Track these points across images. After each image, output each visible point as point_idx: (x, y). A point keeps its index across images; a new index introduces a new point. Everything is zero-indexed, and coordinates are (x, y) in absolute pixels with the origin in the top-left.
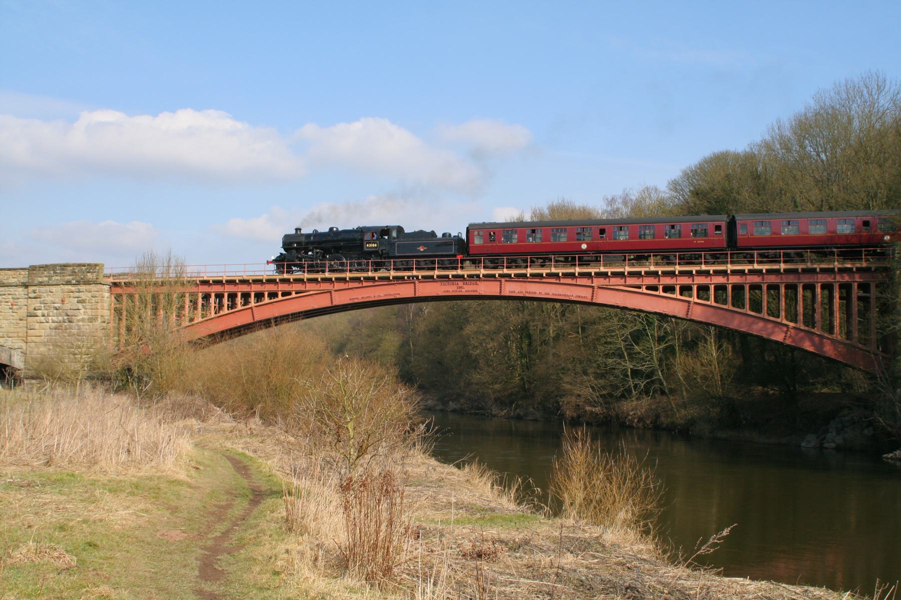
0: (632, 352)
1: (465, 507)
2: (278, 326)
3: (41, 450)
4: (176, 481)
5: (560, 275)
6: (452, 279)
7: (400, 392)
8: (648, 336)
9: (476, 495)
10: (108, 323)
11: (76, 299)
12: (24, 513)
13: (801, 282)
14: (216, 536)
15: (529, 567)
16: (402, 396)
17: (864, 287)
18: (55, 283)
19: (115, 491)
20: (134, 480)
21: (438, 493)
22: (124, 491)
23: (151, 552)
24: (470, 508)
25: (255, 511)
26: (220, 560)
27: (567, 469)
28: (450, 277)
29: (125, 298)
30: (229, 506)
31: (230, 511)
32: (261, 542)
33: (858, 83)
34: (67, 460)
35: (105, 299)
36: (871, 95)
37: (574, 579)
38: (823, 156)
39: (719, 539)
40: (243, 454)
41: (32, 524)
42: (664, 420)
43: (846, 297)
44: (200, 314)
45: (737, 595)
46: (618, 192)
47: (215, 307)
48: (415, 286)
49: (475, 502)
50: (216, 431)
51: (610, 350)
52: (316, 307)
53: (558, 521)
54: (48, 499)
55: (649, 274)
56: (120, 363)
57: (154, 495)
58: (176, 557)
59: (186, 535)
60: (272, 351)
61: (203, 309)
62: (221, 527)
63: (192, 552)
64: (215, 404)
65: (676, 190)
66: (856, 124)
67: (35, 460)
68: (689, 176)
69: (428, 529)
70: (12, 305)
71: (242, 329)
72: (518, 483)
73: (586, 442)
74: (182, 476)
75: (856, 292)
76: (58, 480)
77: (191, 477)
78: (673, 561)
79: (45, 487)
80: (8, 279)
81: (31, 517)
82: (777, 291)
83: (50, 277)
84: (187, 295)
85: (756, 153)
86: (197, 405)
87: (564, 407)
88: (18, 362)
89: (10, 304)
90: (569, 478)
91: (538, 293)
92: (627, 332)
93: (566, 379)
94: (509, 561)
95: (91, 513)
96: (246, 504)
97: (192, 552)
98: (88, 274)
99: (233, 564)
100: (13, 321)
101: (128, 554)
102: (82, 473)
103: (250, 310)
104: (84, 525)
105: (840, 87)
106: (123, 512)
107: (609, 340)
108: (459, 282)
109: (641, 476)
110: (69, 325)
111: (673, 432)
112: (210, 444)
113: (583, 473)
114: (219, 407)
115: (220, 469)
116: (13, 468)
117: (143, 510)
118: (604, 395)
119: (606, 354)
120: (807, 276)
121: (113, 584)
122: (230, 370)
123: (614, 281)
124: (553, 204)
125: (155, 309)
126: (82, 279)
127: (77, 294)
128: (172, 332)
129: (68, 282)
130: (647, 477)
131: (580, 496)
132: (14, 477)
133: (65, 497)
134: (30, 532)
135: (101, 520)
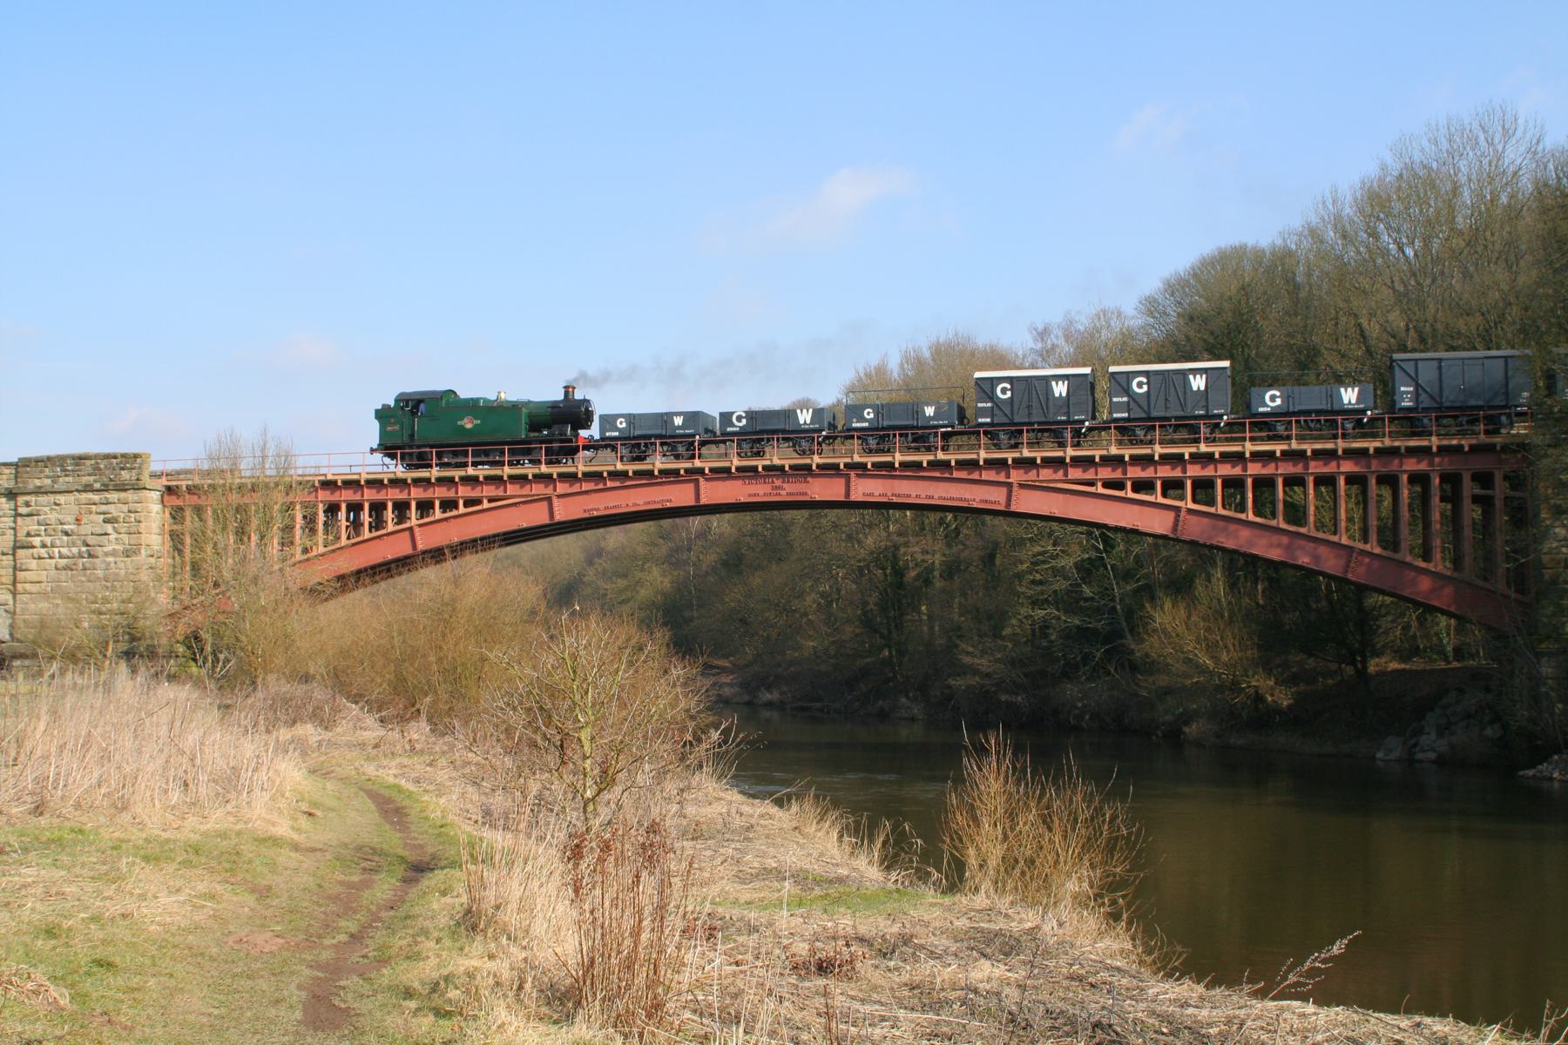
2: (458, 559)
4: (270, 838)
7: (674, 672)
9: (811, 854)
11: (102, 517)
14: (340, 942)
15: (914, 988)
16: (678, 679)
17: (1484, 479)
18: (64, 488)
19: (157, 859)
20: (194, 837)
21: (743, 852)
22: (173, 860)
24: (800, 877)
26: (344, 988)
27: (972, 805)
28: (760, 469)
29: (188, 513)
30: (366, 885)
33: (1471, 124)
35: (153, 515)
36: (1490, 143)
38: (1409, 252)
39: (1324, 961)
43: (1453, 499)
45: (1295, 1035)
46: (1055, 318)
49: (807, 867)
50: (351, 746)
53: (962, 900)
55: (1108, 461)
57: (228, 866)
59: (281, 941)
61: (326, 532)
63: (292, 973)
65: (1151, 314)
66: (1466, 197)
67: (16, 803)
68: (1175, 287)
69: (728, 917)
71: (393, 565)
74: (283, 829)
75: (1469, 488)
77: (298, 830)
78: (1170, 973)
79: (27, 853)
82: (1331, 488)
83: (55, 479)
85: (1293, 247)
90: (976, 821)
91: (914, 495)
94: (876, 977)
95: (108, 903)
97: (292, 973)
98: (123, 472)
99: (368, 997)
101: (172, 980)
102: (99, 827)
103: (407, 534)
104: (92, 927)
106: (168, 900)
107: (1038, 577)
109: (1104, 815)
112: (338, 769)
113: (1000, 811)
114: (356, 703)
117: (205, 894)
123: (1046, 473)
124: (938, 342)
125: (241, 533)
126: (111, 480)
127: (103, 508)
129: (86, 486)
130: (1113, 819)
131: (995, 853)
133: (63, 873)
135: (124, 916)
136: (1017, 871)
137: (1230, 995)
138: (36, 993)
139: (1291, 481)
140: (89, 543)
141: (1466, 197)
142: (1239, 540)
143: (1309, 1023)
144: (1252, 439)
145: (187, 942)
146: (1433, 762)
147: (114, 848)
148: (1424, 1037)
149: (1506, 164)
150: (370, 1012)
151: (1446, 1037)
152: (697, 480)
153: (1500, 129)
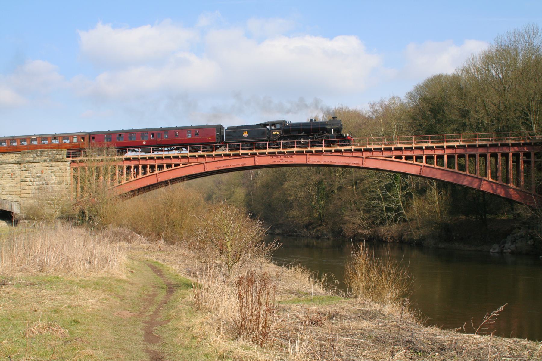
0: (386, 196)
1: (295, 292)
2: (173, 185)
3: (37, 262)
5: (343, 151)
6: (277, 154)
8: (396, 187)
9: (300, 285)
10: (70, 185)
11: (50, 171)
12: (31, 302)
13: (489, 153)
14: (151, 314)
15: (343, 329)
17: (527, 155)
18: (37, 161)
20: (96, 280)
22: (90, 287)
23: (112, 325)
24: (298, 293)
25: (172, 298)
26: (156, 329)
28: (276, 153)
29: (79, 169)
30: (155, 295)
31: (156, 298)
32: (180, 318)
33: (522, 31)
34: (53, 268)
35: (67, 170)
37: (373, 337)
38: (501, 76)
40: (157, 262)
41: (37, 309)
42: (406, 237)
43: (517, 162)
44: (125, 179)
45: (474, 345)
46: (377, 100)
47: (134, 174)
48: (255, 159)
50: (138, 249)
51: (373, 195)
52: (195, 173)
54: (44, 293)
55: (397, 149)
56: (78, 208)
58: (129, 328)
59: (132, 314)
60: (170, 200)
62: (152, 308)
63: (138, 324)
64: (136, 232)
66: (521, 56)
67: (33, 269)
68: (419, 89)
70: (11, 175)
71: (151, 187)
72: (325, 277)
73: (365, 251)
74: (124, 277)
75: (522, 159)
76: (49, 281)
78: (429, 324)
80: (9, 159)
81: (36, 305)
82: (474, 158)
83: (34, 158)
84: (117, 167)
85: (460, 75)
86: (126, 233)
87: (345, 230)
88: (16, 210)
89: (10, 174)
90: (356, 273)
91: (329, 162)
92: (383, 185)
93: (346, 214)
96: (164, 293)
97: (138, 324)
99: (165, 332)
100: (12, 185)
102: (63, 276)
104: (69, 309)
105: (510, 33)
108: (281, 156)
109: (400, 271)
110: (46, 187)
111: (412, 245)
115: (145, 272)
116: (21, 274)
118: (370, 223)
119: (370, 198)
120: (493, 149)
121: (93, 347)
122: (144, 211)
123: (375, 154)
125: (98, 176)
127: (51, 168)
128: (109, 189)
129: (45, 160)
130: (403, 272)
131: (362, 285)
132: (21, 280)
133: (55, 292)
134: (36, 314)
135: (79, 306)
136: (370, 290)
137: (450, 332)
138: (57, 331)
139: (460, 156)
140: (46, 180)
141: (521, 56)
142: (438, 175)
143: (479, 341)
144: (446, 141)
145: (101, 314)
146: (510, 253)
147: (69, 283)
148: (518, 346)
149: (534, 45)
150: (167, 337)
151: (526, 346)
152: (254, 157)
153: (532, 33)
